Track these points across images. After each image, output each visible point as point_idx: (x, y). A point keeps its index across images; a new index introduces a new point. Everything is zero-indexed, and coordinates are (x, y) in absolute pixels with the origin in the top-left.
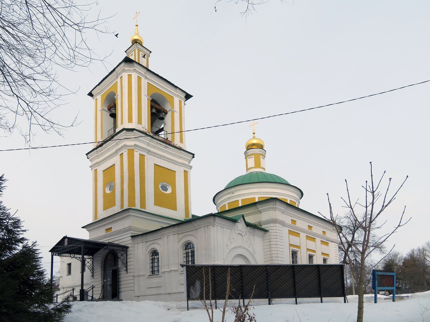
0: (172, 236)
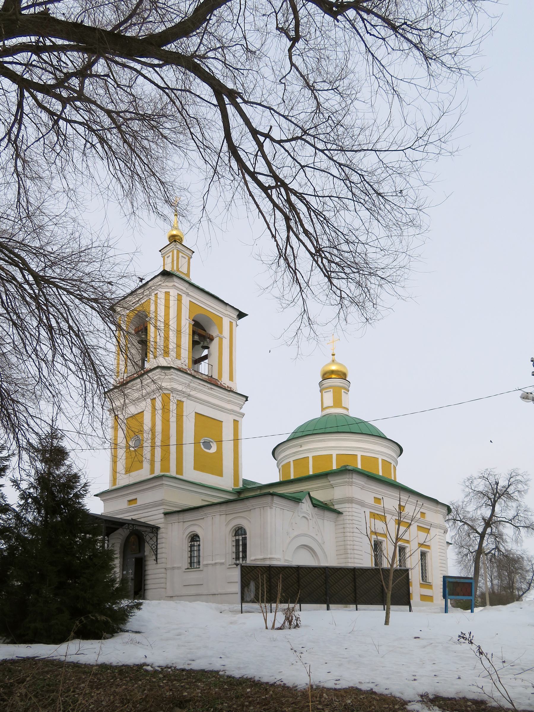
0: (217, 518)
